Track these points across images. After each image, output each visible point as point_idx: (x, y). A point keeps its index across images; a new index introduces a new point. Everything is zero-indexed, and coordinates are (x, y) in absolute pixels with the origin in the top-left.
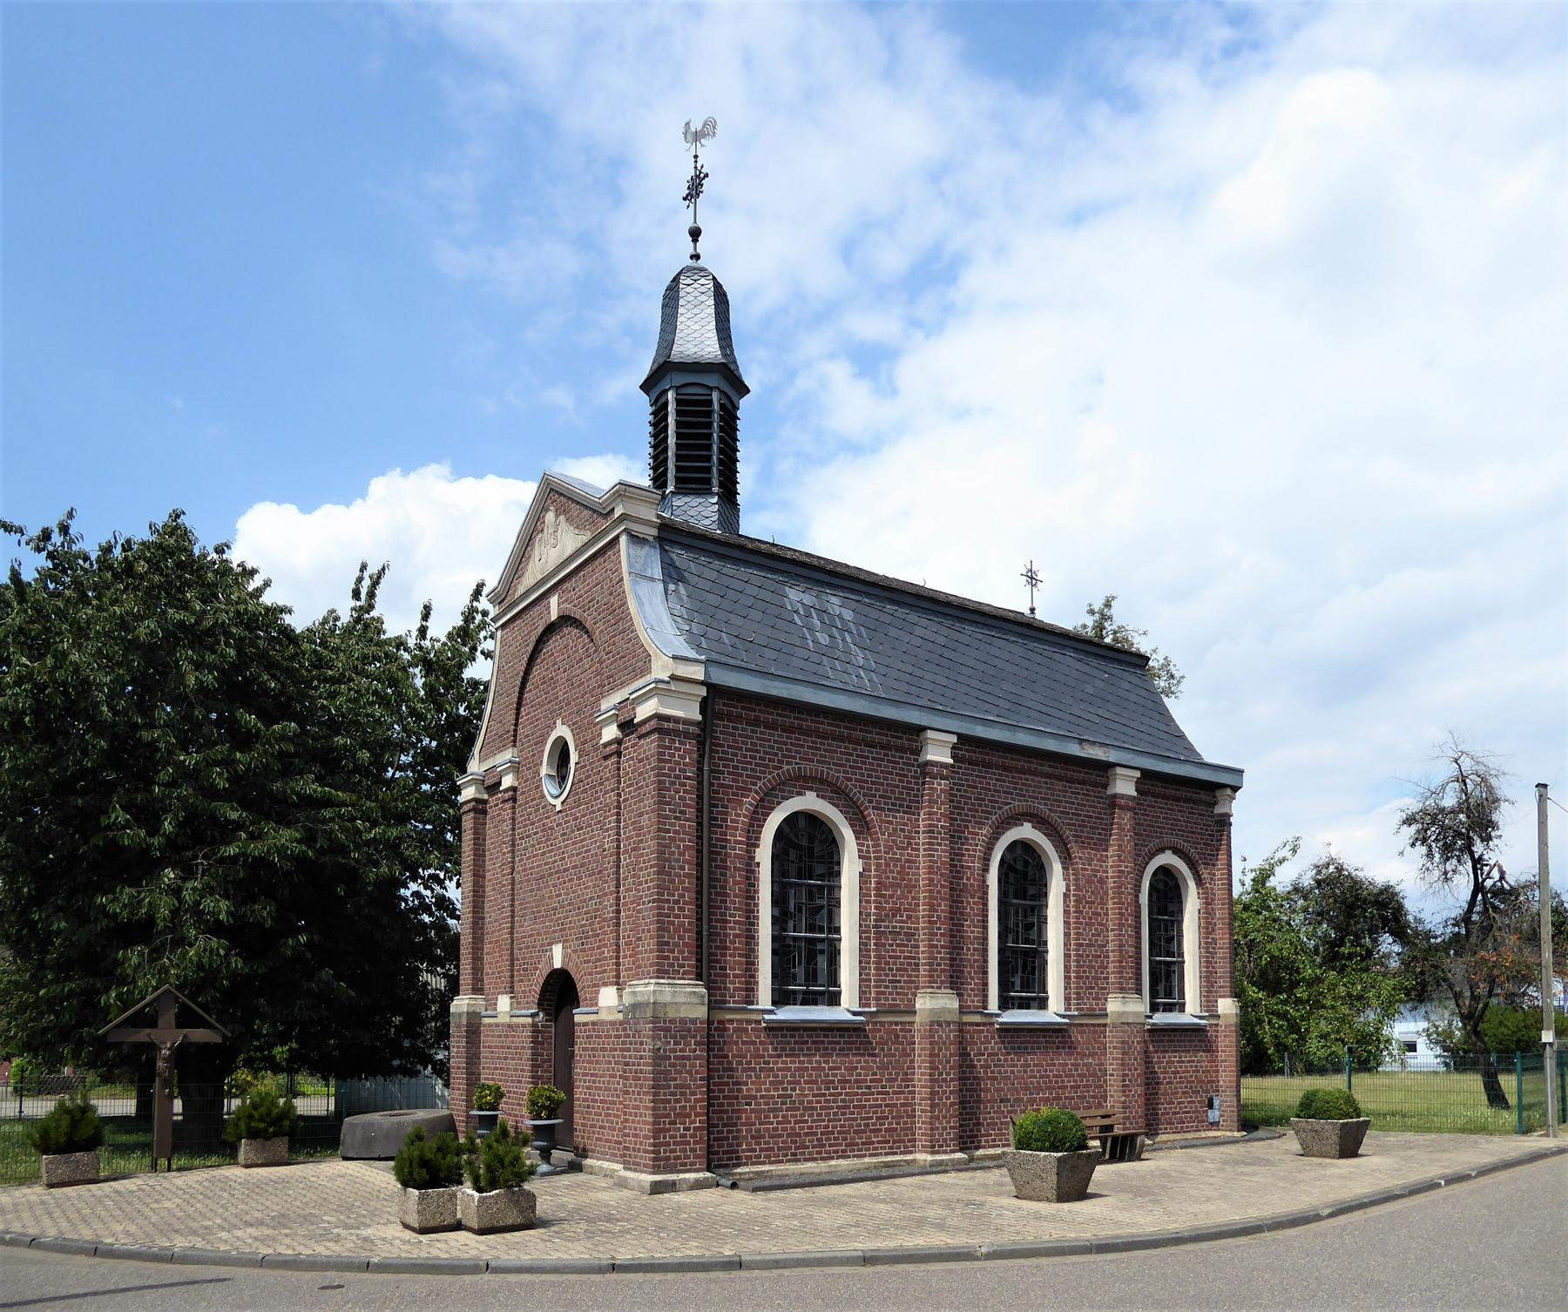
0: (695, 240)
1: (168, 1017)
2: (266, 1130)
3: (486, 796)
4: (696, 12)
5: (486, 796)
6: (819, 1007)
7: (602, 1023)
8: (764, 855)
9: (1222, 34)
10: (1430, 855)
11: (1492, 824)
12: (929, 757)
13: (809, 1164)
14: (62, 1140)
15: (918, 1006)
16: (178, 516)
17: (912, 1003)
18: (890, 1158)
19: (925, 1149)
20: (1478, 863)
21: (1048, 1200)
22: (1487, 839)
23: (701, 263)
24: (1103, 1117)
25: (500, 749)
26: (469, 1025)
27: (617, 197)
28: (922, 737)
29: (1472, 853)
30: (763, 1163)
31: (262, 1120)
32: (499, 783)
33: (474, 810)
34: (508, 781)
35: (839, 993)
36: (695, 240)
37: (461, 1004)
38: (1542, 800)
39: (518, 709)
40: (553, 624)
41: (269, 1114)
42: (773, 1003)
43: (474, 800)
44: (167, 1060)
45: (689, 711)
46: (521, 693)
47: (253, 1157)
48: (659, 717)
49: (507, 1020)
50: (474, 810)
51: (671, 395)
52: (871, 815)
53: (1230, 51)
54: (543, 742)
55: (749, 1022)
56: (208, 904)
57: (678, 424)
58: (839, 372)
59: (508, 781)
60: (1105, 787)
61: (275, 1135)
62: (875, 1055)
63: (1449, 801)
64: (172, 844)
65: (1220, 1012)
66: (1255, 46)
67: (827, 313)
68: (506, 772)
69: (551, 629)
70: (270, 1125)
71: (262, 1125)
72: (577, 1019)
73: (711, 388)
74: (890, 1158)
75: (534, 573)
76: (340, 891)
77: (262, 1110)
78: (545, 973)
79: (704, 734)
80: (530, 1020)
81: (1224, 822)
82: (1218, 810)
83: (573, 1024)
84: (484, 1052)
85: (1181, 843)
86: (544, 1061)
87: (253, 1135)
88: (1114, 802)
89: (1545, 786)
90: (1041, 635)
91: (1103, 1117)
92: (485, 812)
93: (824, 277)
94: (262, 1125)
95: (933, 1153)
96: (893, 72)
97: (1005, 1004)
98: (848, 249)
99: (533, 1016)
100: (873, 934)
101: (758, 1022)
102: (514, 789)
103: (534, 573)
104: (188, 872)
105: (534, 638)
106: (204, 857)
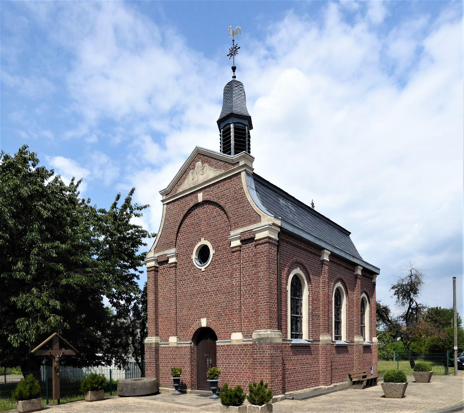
0: (234, 71)
1: (56, 346)
2: (98, 387)
3: (158, 266)
4: (98, 7)
5: (158, 266)
6: (299, 339)
7: (233, 345)
8: (289, 288)
9: (263, 52)
10: (398, 297)
11: (417, 290)
12: (325, 258)
13: (300, 391)
14: (28, 394)
15: (321, 339)
16: (26, 148)
17: (319, 337)
18: (316, 388)
19: (324, 384)
20: (411, 300)
21: (398, 398)
22: (415, 293)
23: (236, 79)
24: (364, 373)
25: (170, 248)
26: (156, 347)
27: (70, 68)
28: (322, 251)
29: (410, 298)
30: (290, 391)
31: (96, 384)
32: (168, 261)
33: (155, 270)
34: (172, 260)
35: (302, 335)
36: (234, 71)
37: (150, 340)
38: (454, 282)
39: (177, 234)
40: (199, 203)
41: (98, 382)
42: (291, 338)
43: (154, 266)
44: (57, 362)
45: (275, 236)
46: (179, 228)
47: (93, 398)
48: (268, 237)
49: (175, 345)
50: (155, 270)
51: (232, 126)
52: (311, 277)
53: (266, 58)
54: (193, 245)
55: (287, 344)
56: (52, 302)
57: (235, 137)
58: (148, 139)
59: (172, 260)
60: (354, 271)
61: (100, 389)
62: (312, 355)
63: (405, 282)
64: (34, 279)
65: (373, 341)
66: (274, 58)
67: (144, 119)
68: (172, 257)
69: (197, 205)
70: (99, 385)
71: (97, 385)
72: (217, 344)
73: (245, 125)
74: (316, 388)
75: (187, 184)
76: (90, 299)
77: (96, 380)
78: (196, 328)
79: (278, 245)
80: (189, 345)
81: (374, 284)
82: (373, 281)
83: (216, 346)
84: (161, 357)
85: (367, 291)
86: (194, 359)
87: (93, 389)
88: (356, 277)
89: (455, 278)
90: (331, 223)
91: (364, 373)
92: (157, 271)
93: (142, 107)
94: (97, 385)
95: (327, 385)
96: (164, 44)
97: (292, 335)
98: (150, 99)
99: (191, 343)
100: (312, 315)
101: (289, 344)
102: (176, 263)
103: (187, 184)
104: (41, 291)
105: (187, 208)
106: (46, 284)
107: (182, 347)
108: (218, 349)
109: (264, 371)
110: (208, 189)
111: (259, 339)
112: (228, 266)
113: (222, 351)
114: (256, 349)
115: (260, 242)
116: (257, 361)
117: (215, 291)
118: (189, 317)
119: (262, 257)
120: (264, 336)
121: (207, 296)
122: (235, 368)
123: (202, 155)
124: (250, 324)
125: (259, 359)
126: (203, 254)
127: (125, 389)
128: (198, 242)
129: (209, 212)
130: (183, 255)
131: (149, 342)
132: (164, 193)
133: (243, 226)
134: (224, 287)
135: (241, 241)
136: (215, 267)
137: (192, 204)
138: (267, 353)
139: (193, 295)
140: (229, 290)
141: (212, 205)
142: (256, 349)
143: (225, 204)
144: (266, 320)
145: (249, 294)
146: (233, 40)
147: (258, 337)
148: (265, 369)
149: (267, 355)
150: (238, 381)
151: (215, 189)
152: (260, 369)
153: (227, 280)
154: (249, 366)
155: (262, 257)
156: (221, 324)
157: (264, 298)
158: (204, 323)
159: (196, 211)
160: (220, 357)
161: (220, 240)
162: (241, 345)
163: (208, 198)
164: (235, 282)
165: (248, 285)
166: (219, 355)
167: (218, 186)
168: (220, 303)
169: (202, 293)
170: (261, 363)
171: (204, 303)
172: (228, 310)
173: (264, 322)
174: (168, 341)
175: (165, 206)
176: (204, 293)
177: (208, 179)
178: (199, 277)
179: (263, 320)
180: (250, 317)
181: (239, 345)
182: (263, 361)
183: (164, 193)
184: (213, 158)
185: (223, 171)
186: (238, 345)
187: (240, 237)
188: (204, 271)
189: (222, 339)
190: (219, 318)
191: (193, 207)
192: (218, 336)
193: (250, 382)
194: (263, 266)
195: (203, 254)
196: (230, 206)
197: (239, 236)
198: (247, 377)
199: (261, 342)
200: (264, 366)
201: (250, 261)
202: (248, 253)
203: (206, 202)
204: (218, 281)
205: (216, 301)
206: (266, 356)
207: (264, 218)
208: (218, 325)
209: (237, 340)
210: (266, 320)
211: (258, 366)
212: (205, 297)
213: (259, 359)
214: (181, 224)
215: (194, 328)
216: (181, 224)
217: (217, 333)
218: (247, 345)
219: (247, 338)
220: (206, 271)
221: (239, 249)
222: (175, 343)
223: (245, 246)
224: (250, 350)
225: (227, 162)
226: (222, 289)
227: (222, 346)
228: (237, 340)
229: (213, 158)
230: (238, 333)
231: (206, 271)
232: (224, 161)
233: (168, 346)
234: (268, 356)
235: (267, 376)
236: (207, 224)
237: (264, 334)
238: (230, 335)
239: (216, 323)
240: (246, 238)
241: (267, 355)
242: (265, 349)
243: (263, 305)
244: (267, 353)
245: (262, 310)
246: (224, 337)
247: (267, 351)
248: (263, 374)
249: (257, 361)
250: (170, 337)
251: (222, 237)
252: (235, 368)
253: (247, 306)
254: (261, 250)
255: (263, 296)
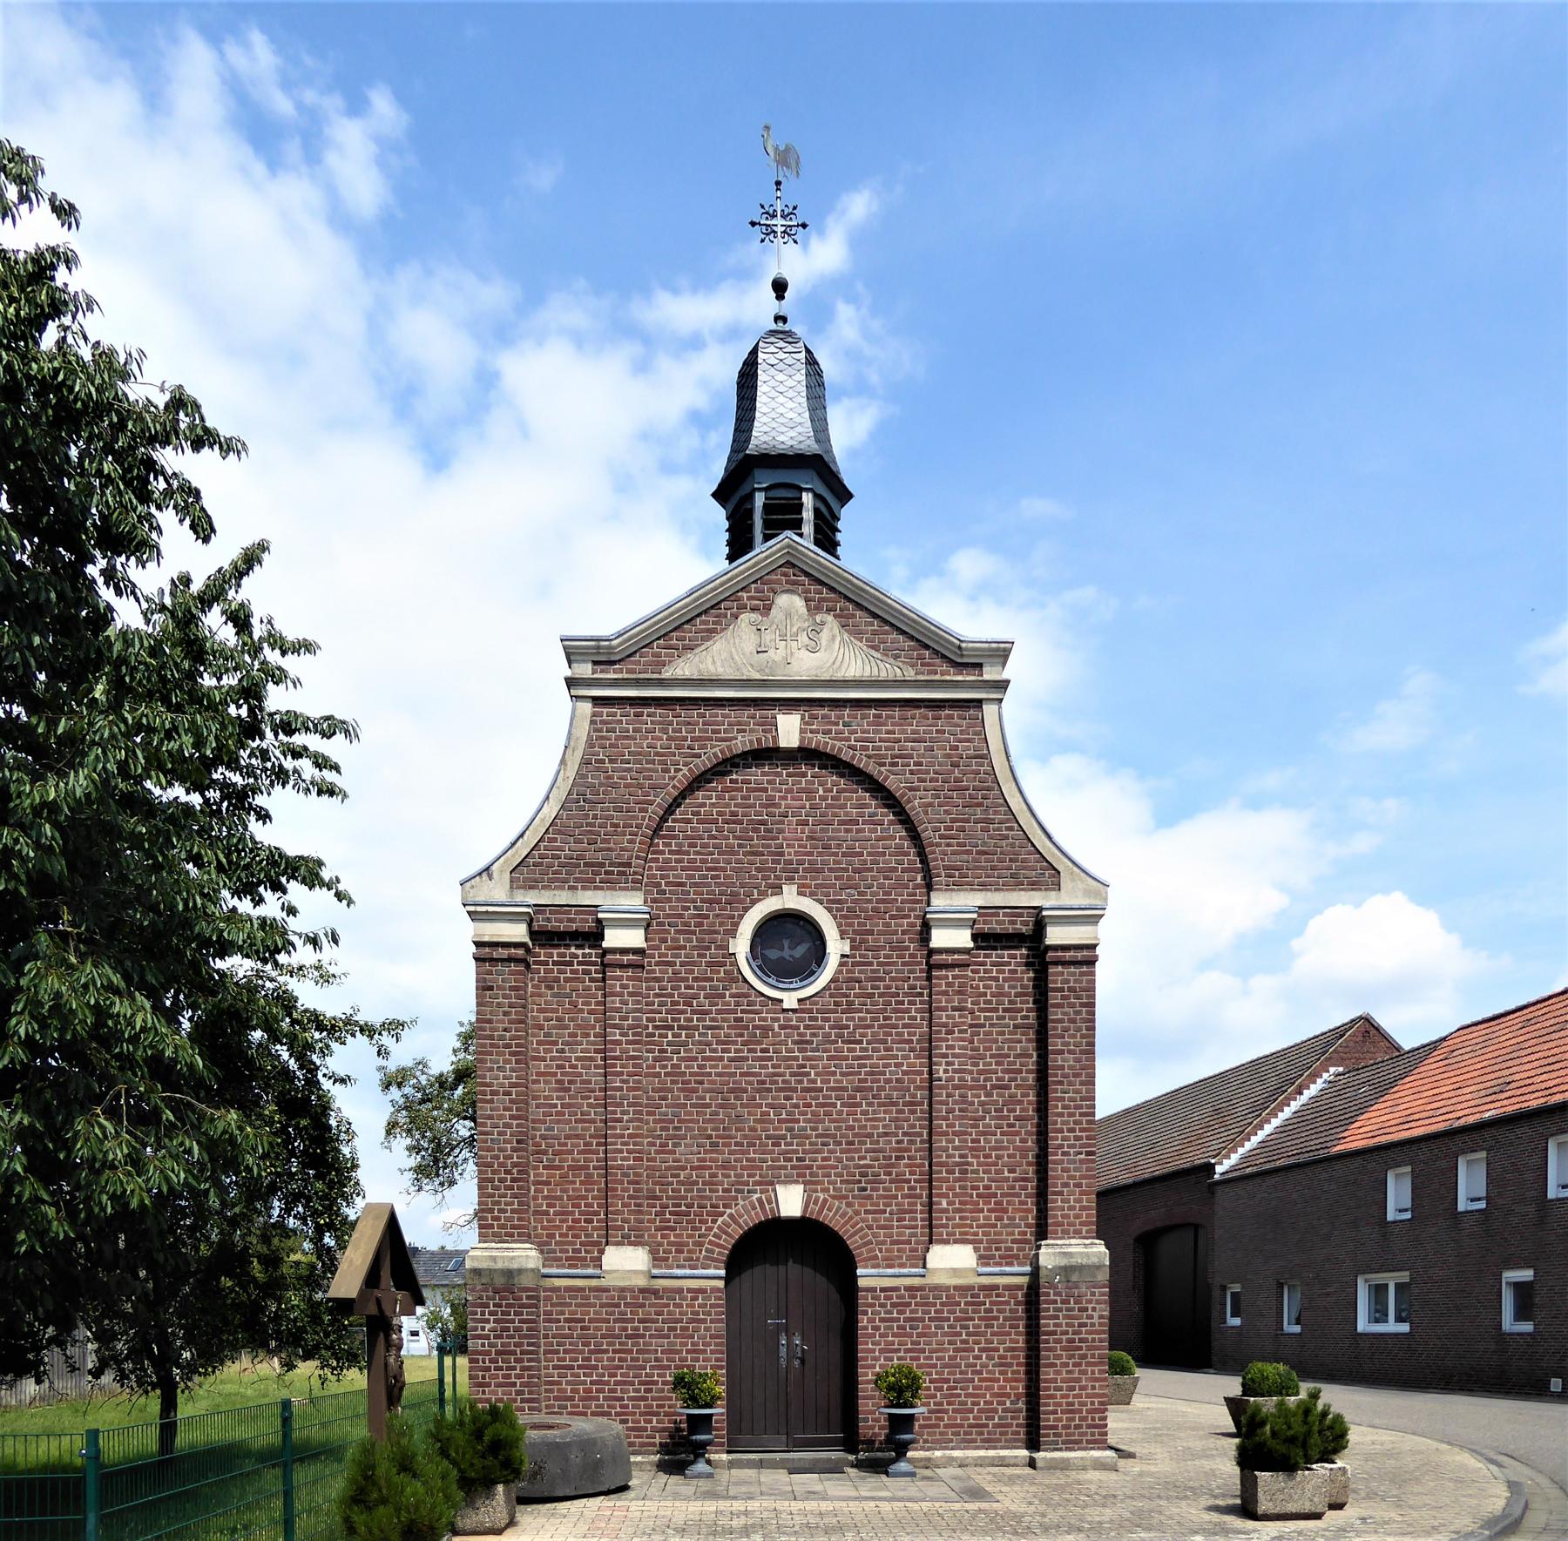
0: (780, 297)
7: (936, 1288)
36: (780, 297)
40: (777, 749)
49: (642, 1282)
69: (767, 755)
72: (862, 1283)
78: (749, 1220)
107: (680, 1291)
108: (863, 1299)
109: (1081, 1372)
110: (825, 711)
111: (1067, 1270)
112: (908, 1011)
113: (881, 1305)
114: (1055, 1302)
115: (1069, 955)
116: (1059, 1341)
117: (844, 1089)
118: (713, 1175)
119: (1072, 1005)
120: (1085, 1261)
121: (810, 1105)
122: (946, 1366)
123: (807, 574)
124: (1000, 1219)
125: (1066, 1333)
126: (790, 946)
127: (552, 1468)
128: (764, 895)
129: (824, 798)
130: (688, 925)
131: (500, 1265)
132: (591, 658)
133: (984, 887)
134: (888, 1081)
135: (975, 937)
136: (850, 1003)
137: (742, 743)
138: (1096, 1314)
139: (732, 1091)
140: (914, 1096)
141: (842, 775)
142: (1055, 1302)
143: (911, 789)
144: (1083, 1208)
145: (998, 1118)
146: (778, 183)
147: (1064, 1262)
148: (1088, 1364)
149: (1096, 1320)
150: (954, 1411)
151: (862, 723)
152: (1067, 1365)
153: (905, 1057)
154: (1000, 1357)
155: (1072, 1005)
156: (875, 1212)
157: (1077, 1138)
158: (791, 1202)
159: (757, 775)
160: (877, 1328)
161: (874, 910)
162: (970, 1288)
163: (818, 740)
164: (946, 1071)
165: (994, 1087)
166: (871, 1321)
167: (875, 716)
168: (870, 1135)
169: (780, 1090)
170: (1071, 1347)
171: (791, 1130)
172: (906, 1166)
173: (1077, 1216)
174: (598, 1263)
175: (586, 708)
176: (794, 1090)
177: (839, 676)
178: (766, 1030)
179: (1071, 1208)
180: (1003, 1195)
181: (963, 1289)
182: (1081, 1340)
183: (591, 658)
184: (859, 606)
185: (910, 674)
186: (956, 1288)
187: (974, 921)
188: (794, 1011)
189: (902, 1266)
190: (865, 1189)
191: (744, 755)
192: (860, 1253)
193: (1004, 1410)
194: (1074, 1036)
195: (790, 946)
196: (931, 805)
197: (975, 916)
198: (993, 1395)
199: (1074, 1278)
200: (1084, 1357)
201: (1005, 1010)
202: (996, 979)
203: (807, 755)
204: (860, 1058)
205: (852, 1128)
206: (1093, 1325)
207: (1073, 880)
208: (857, 1213)
209: (955, 1272)
210: (1083, 1208)
211: (1059, 1357)
212: (796, 1106)
213: (1066, 1333)
214: (676, 803)
215: (743, 1215)
216: (676, 803)
217: (853, 1243)
218: (995, 1287)
219: (988, 1265)
220: (803, 1011)
221: (957, 960)
222: (635, 1272)
223: (986, 956)
224: (1007, 1303)
225: (927, 647)
226: (881, 1089)
227: (883, 1290)
228: (955, 1270)
229: (859, 606)
230: (956, 1246)
231: (803, 1011)
232: (912, 638)
233: (594, 1283)
234: (1101, 1324)
235: (1093, 1388)
236: (810, 838)
237: (1087, 1254)
238: (602, 1252)
239: (849, 1205)
240: (998, 929)
241: (1096, 1320)
242: (1090, 1302)
243: (1074, 1162)
244: (1096, 1314)
245: (1070, 1177)
246: (885, 1259)
247: (1094, 1309)
248: (1078, 1380)
249: (1059, 1341)
250: (610, 1250)
251: (883, 901)
252: (946, 1366)
253: (990, 1156)
254: (1067, 982)
255: (1072, 1130)
